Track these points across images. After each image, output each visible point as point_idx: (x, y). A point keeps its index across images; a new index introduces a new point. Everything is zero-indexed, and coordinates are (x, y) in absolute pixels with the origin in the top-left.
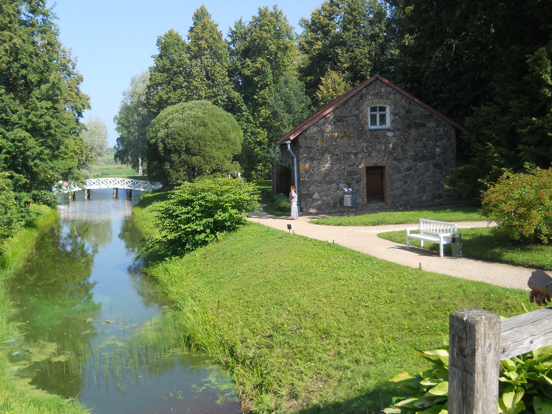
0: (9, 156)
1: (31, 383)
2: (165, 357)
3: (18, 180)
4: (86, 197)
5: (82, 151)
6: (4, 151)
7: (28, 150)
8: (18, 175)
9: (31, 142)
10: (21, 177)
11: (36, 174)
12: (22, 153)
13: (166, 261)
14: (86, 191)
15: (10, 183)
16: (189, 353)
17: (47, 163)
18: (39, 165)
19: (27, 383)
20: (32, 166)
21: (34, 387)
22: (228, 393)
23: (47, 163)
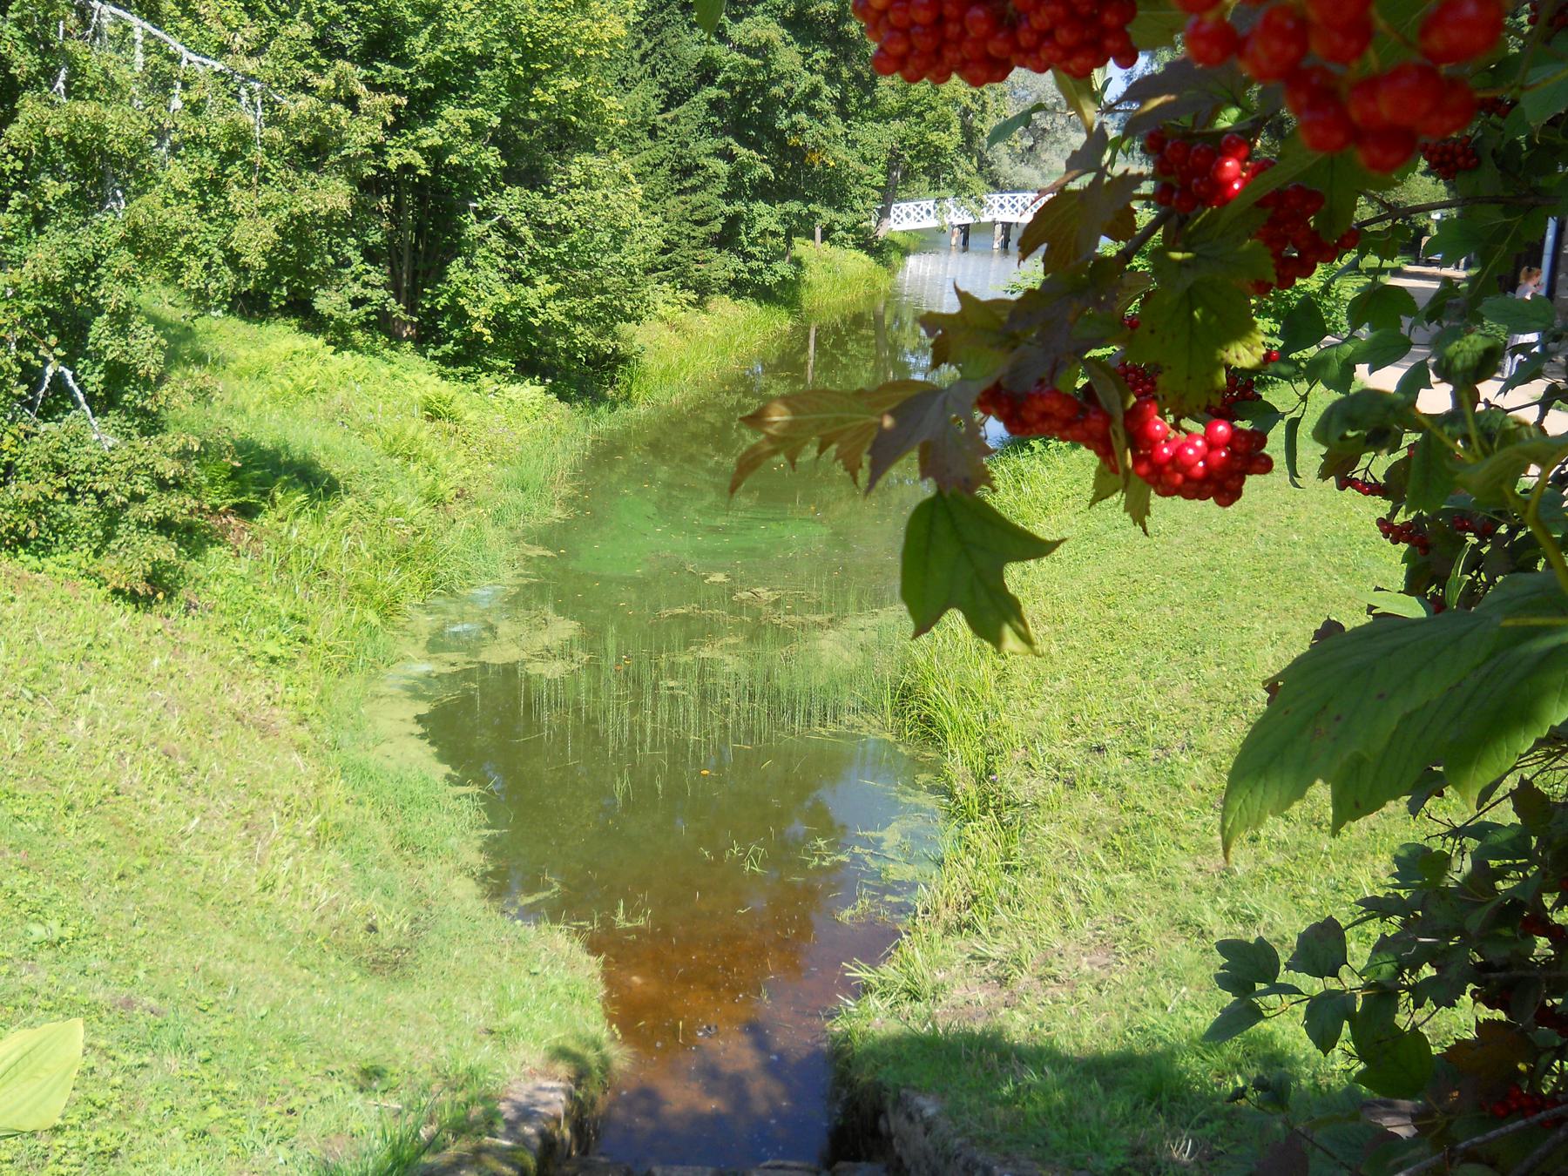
0: (728, 95)
1: (419, 719)
2: (819, 734)
3: (745, 168)
4: (996, 245)
5: (984, 105)
6: (720, 78)
7: (774, 82)
8: (744, 151)
9: (788, 57)
10: (753, 158)
11: (799, 153)
12: (762, 89)
13: (1032, 449)
14: (999, 228)
15: (721, 173)
16: (893, 739)
17: (827, 125)
18: (803, 130)
19: (410, 716)
20: (783, 132)
21: (419, 729)
22: (898, 894)
23: (827, 125)
